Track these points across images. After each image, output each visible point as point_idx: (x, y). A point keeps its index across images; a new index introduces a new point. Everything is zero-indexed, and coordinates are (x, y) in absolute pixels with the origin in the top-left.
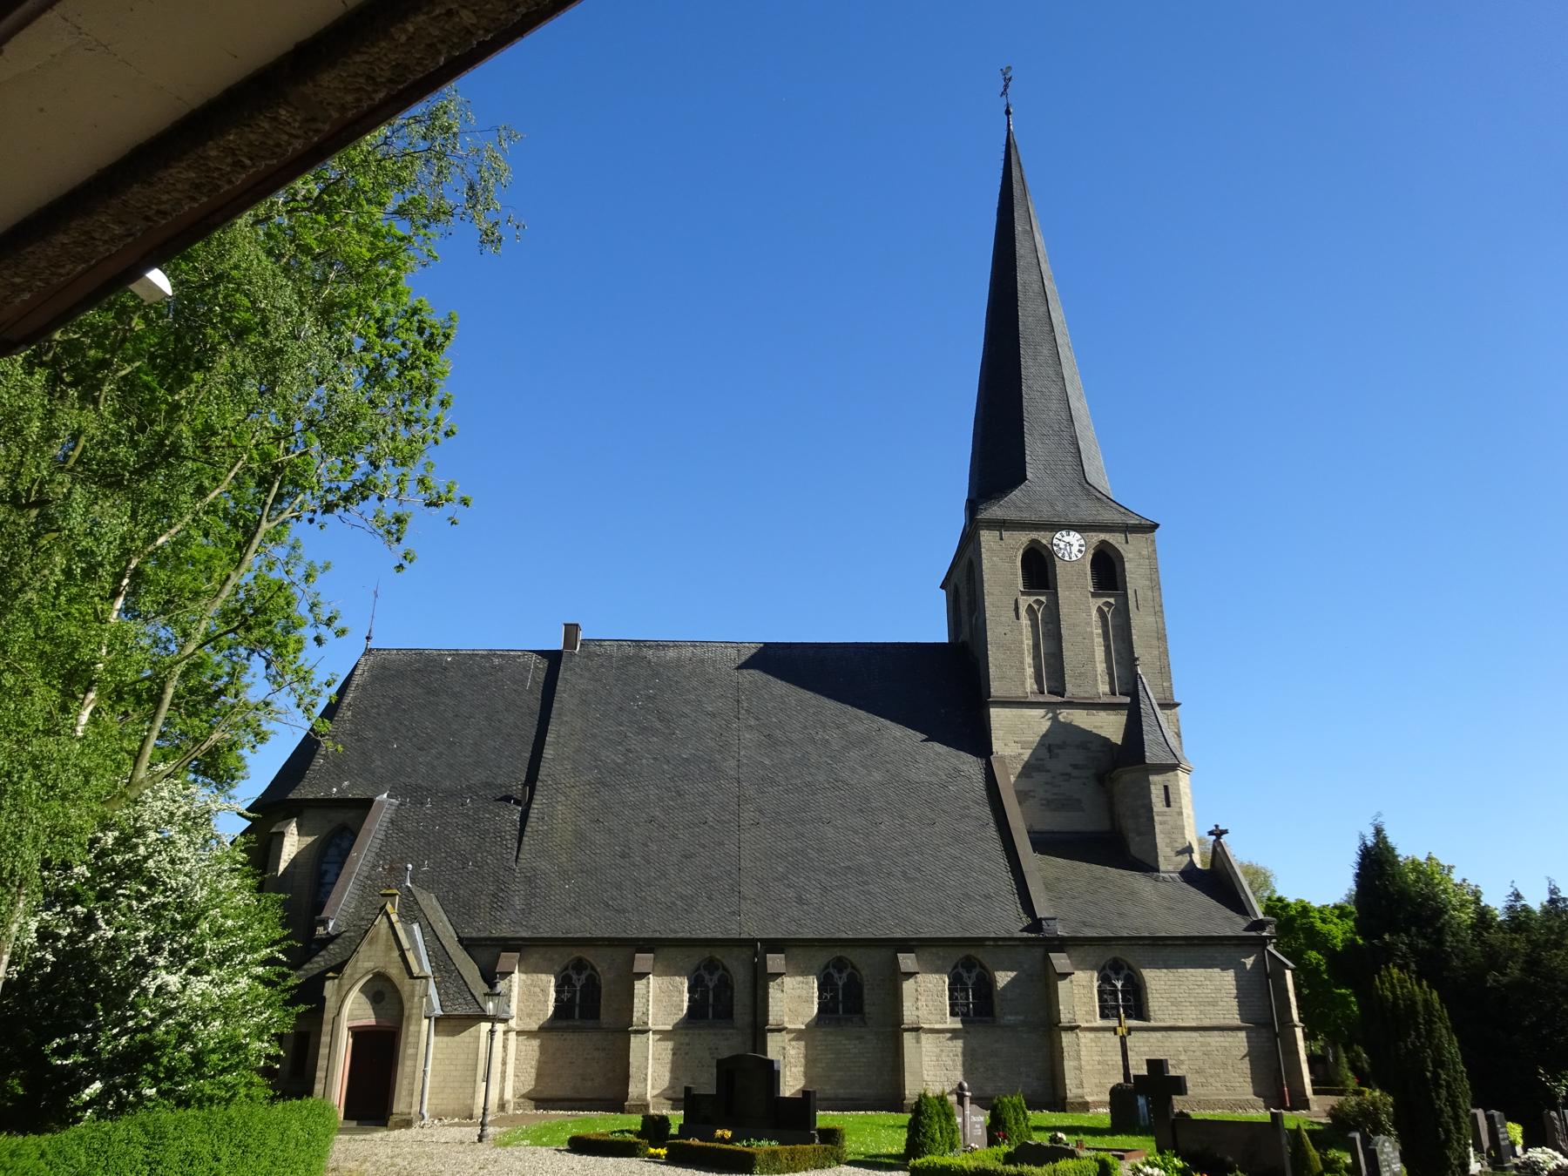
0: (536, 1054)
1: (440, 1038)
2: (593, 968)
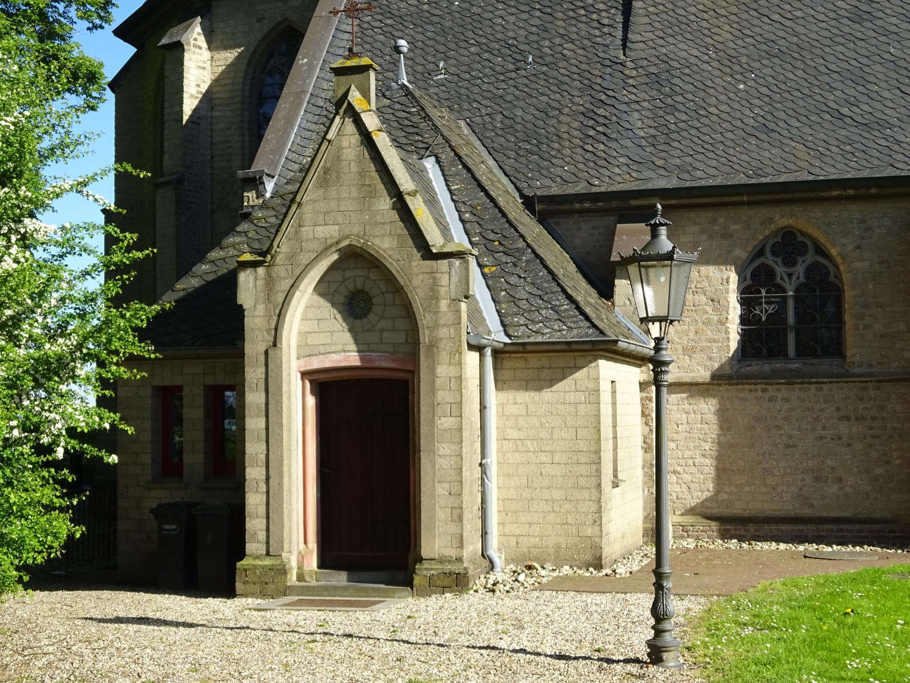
0: (712, 429)
1: (500, 394)
2: (820, 250)
